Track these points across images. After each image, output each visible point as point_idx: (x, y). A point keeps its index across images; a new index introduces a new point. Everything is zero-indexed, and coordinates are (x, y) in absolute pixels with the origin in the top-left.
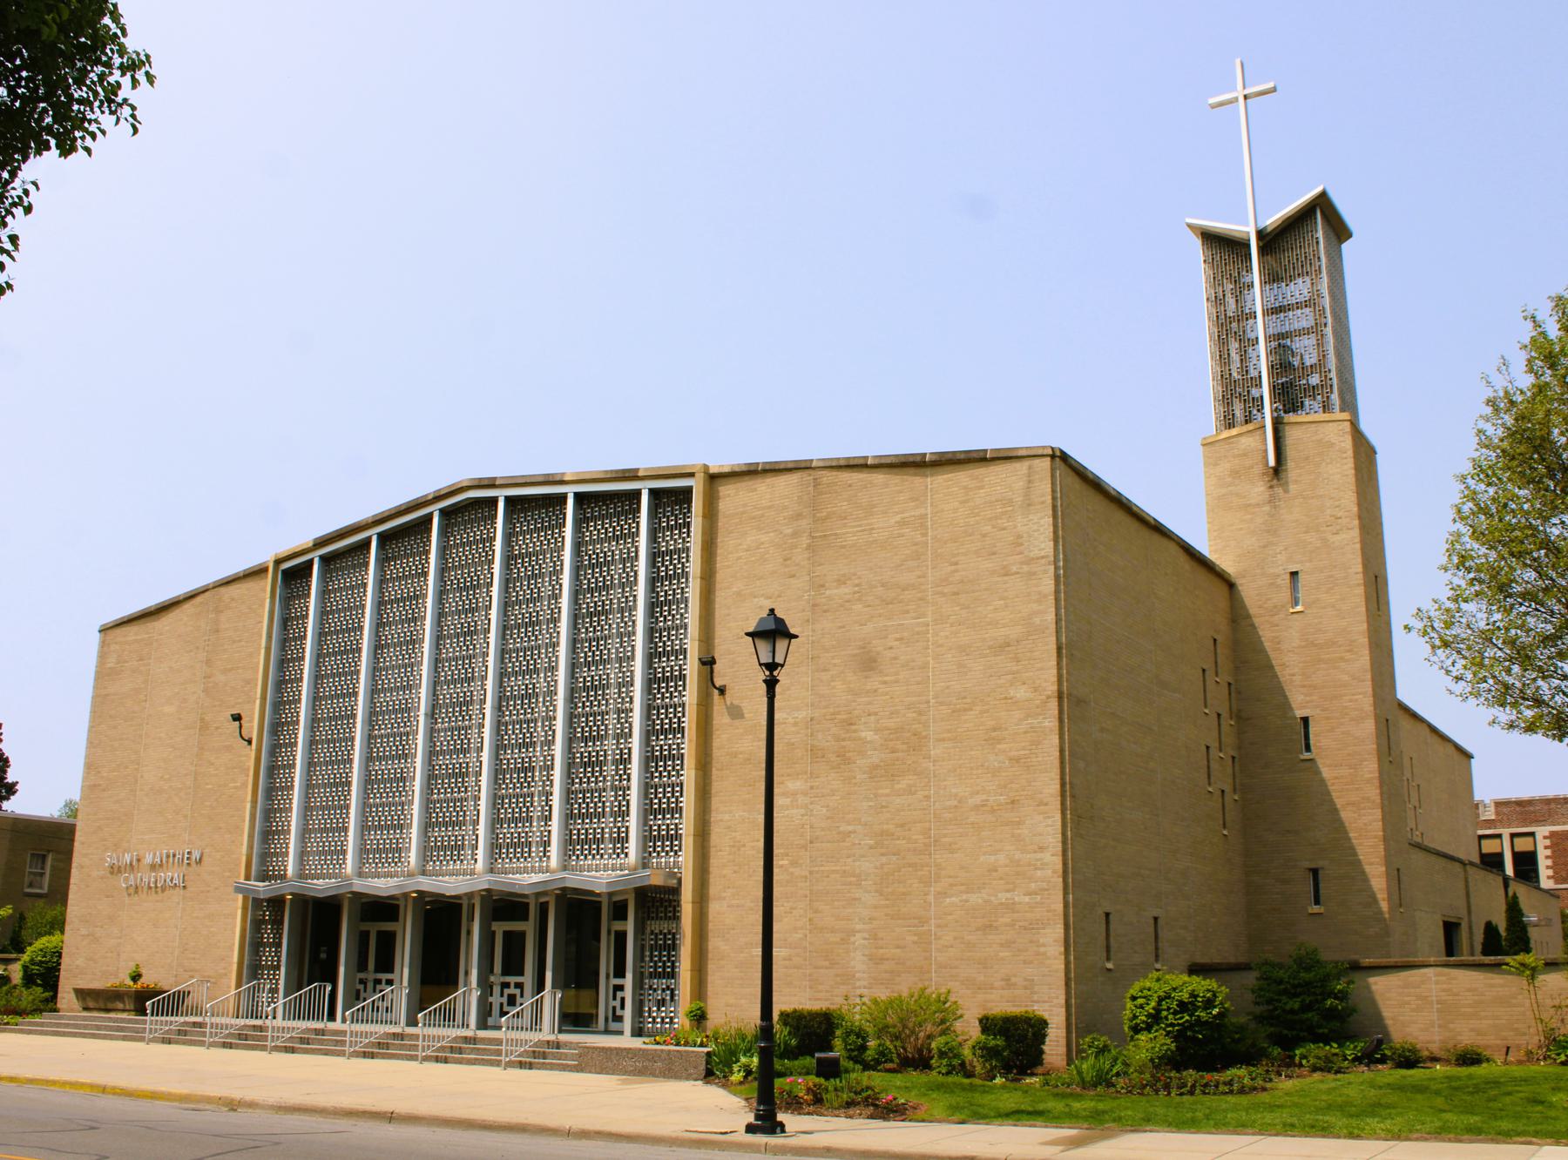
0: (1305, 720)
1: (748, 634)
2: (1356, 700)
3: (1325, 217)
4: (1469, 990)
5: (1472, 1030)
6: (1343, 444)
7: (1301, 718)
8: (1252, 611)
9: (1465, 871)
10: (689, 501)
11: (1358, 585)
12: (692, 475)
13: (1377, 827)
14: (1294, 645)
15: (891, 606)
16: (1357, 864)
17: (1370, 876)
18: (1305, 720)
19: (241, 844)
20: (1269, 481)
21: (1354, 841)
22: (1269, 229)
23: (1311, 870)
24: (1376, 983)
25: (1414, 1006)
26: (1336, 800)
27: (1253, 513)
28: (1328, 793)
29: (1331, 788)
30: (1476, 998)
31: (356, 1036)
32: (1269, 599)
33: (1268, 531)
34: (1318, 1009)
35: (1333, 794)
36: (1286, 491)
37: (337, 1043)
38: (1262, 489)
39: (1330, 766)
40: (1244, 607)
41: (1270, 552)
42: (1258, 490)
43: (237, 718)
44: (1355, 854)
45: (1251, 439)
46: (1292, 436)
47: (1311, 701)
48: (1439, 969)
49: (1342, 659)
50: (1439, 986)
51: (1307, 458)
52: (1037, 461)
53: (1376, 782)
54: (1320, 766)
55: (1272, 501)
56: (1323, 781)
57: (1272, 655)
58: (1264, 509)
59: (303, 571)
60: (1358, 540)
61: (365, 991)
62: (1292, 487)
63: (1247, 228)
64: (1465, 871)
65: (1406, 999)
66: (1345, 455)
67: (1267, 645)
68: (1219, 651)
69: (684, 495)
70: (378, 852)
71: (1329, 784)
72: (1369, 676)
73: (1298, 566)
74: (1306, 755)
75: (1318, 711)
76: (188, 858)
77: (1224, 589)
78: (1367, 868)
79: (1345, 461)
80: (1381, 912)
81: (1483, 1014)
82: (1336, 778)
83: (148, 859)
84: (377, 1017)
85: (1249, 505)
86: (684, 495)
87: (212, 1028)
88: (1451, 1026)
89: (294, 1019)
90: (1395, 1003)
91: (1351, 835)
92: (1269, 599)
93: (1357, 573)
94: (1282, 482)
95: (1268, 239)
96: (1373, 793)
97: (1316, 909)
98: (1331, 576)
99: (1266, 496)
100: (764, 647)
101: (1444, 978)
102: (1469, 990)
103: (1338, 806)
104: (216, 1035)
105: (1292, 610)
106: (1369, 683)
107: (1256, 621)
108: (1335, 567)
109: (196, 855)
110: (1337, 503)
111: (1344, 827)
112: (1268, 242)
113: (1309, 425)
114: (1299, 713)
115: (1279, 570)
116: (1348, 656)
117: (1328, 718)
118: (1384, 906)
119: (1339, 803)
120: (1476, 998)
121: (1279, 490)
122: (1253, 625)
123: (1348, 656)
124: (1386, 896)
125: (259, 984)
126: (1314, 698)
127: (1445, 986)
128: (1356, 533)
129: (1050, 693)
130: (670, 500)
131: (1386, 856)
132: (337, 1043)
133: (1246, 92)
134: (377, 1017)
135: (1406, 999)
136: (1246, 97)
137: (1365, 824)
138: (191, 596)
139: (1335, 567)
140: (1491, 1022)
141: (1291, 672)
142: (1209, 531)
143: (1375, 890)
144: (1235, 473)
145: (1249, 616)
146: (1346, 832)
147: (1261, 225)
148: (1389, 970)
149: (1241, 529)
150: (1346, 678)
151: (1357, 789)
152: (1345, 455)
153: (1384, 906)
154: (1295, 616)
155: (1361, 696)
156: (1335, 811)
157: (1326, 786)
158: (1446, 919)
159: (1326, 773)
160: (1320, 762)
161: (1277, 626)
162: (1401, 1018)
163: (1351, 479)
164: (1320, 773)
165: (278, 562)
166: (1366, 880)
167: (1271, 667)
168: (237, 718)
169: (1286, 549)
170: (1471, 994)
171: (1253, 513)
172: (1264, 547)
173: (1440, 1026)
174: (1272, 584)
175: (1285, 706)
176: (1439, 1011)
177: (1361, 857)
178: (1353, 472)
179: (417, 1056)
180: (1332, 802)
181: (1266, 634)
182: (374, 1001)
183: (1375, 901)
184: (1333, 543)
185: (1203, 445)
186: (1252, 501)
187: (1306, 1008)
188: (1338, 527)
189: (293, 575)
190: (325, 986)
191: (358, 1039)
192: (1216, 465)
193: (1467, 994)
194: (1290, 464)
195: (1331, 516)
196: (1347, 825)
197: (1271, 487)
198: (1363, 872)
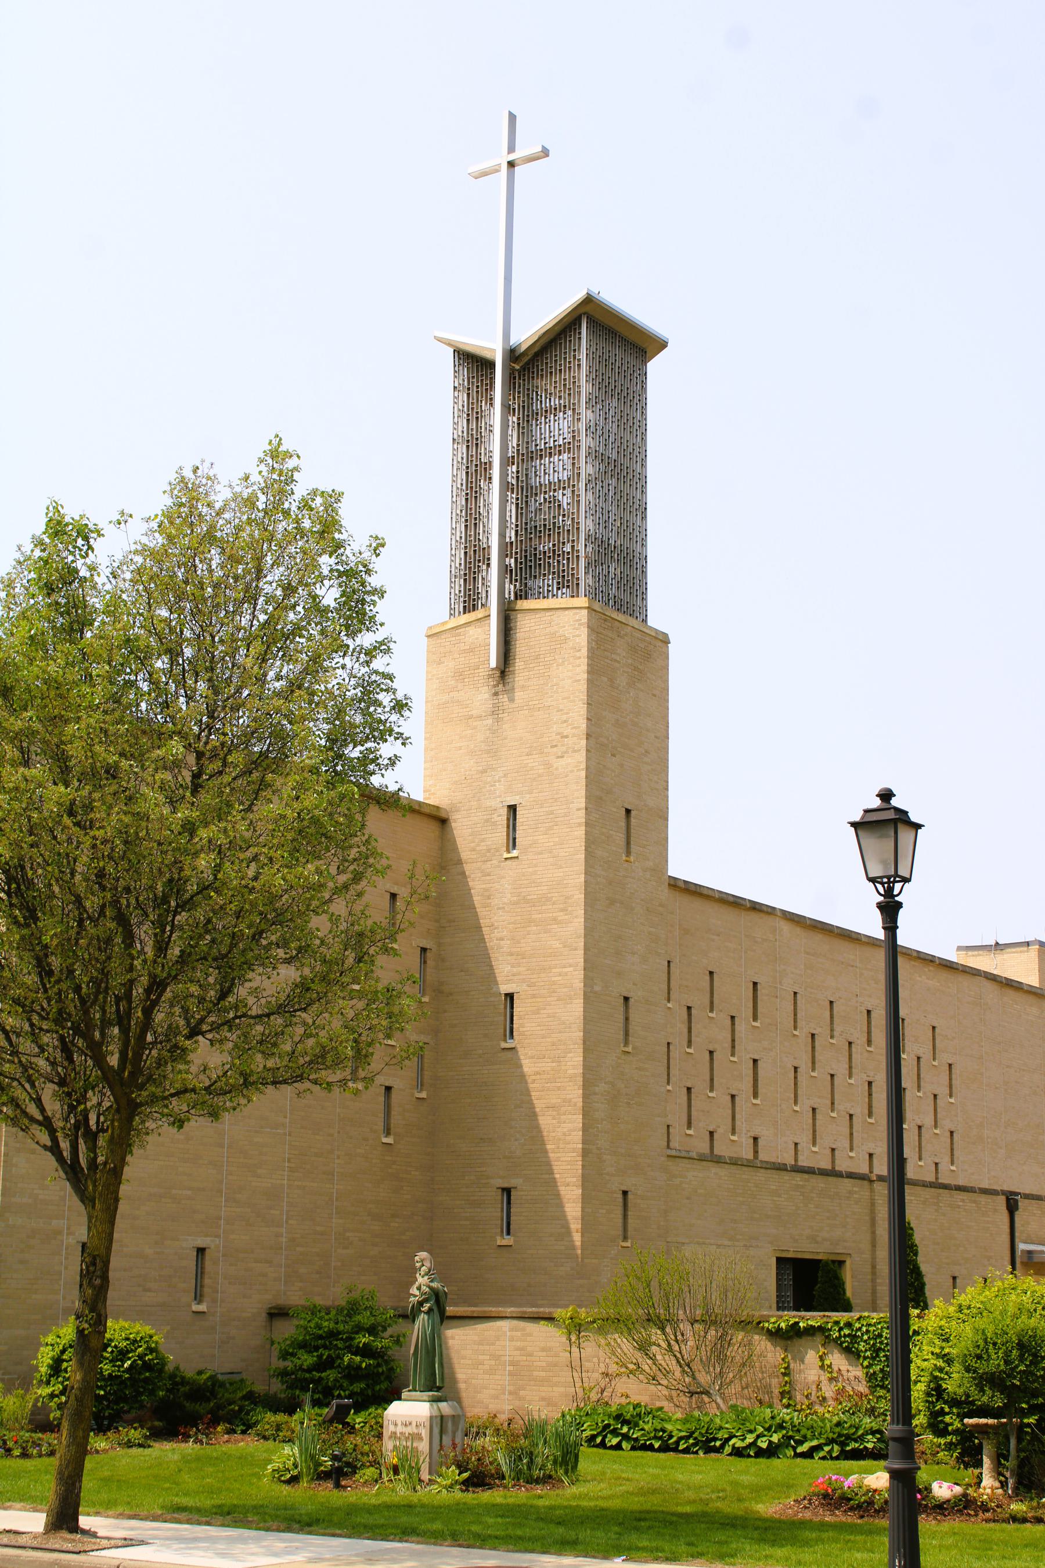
0: (510, 997)
1: (849, 823)
2: (566, 974)
3: (593, 322)
4: (543, 1350)
5: (543, 1399)
6: (577, 640)
7: (506, 995)
8: (465, 855)
9: (872, 1191)
11: (579, 825)
13: (576, 1137)
14: (505, 900)
16: (552, 1183)
17: (565, 1201)
18: (510, 997)
20: (495, 686)
21: (551, 1155)
22: (524, 348)
23: (503, 1189)
24: (453, 1338)
25: (488, 1367)
26: (535, 1102)
27: (475, 728)
28: (527, 1093)
29: (531, 1086)
30: (550, 1359)
32: (483, 840)
33: (488, 752)
34: (339, 1366)
35: (533, 1094)
36: (512, 700)
38: (487, 696)
39: (532, 1057)
40: (455, 849)
41: (489, 779)
42: (481, 696)
44: (551, 1172)
45: (479, 630)
46: (525, 626)
47: (519, 974)
48: (515, 1322)
49: (555, 919)
50: (514, 1343)
51: (537, 657)
53: (580, 1080)
54: (522, 1057)
55: (496, 712)
56: (522, 1077)
57: (481, 911)
58: (485, 722)
60: (583, 766)
62: (518, 695)
63: (494, 349)
64: (872, 1191)
65: (481, 1357)
66: (578, 654)
67: (477, 899)
71: (529, 1081)
72: (581, 944)
73: (517, 797)
74: (509, 1044)
75: (524, 987)
77: (431, 829)
78: (563, 1190)
79: (578, 662)
80: (574, 1248)
81: (555, 1379)
82: (537, 1073)
85: (471, 717)
88: (522, 1393)
90: (470, 1362)
91: (548, 1147)
92: (483, 840)
93: (578, 810)
94: (507, 688)
95: (526, 359)
96: (576, 1094)
97: (508, 1240)
98: (552, 813)
99: (489, 706)
100: (880, 845)
101: (519, 1334)
102: (543, 1350)
103: (537, 1110)
105: (506, 855)
106: (581, 952)
107: (468, 868)
108: (556, 800)
110: (564, 717)
111: (542, 1136)
112: (527, 363)
113: (542, 614)
114: (505, 989)
115: (495, 803)
116: (561, 916)
117: (534, 996)
118: (577, 1238)
119: (539, 1105)
120: (550, 1359)
121: (504, 698)
122: (463, 873)
123: (561, 916)
124: (580, 1226)
126: (521, 969)
127: (519, 1344)
128: (582, 756)
131: (583, 1175)
133: (511, 157)
135: (481, 1357)
136: (511, 164)
137: (564, 1134)
139: (556, 800)
140: (562, 1389)
141: (499, 935)
142: (426, 749)
143: (569, 1218)
144: (459, 675)
145: (459, 862)
146: (543, 1144)
147: (514, 341)
148: (467, 1321)
149: (460, 748)
150: (557, 944)
151: (559, 1088)
152: (578, 654)
153: (577, 1238)
154: (509, 862)
155: (571, 969)
156: (533, 1116)
157: (526, 1083)
158: (779, 1255)
159: (528, 1066)
160: (521, 1052)
161: (489, 875)
162: (474, 1381)
163: (583, 686)
164: (521, 1066)
166: (560, 1205)
167: (479, 928)
169: (505, 776)
170: (544, 1354)
171: (475, 728)
172: (484, 771)
173: (510, 1393)
174: (487, 821)
175: (490, 977)
176: (511, 1374)
177: (557, 1176)
178: (585, 676)
180: (532, 1107)
181: (477, 885)
183: (568, 1232)
184: (557, 769)
185: (428, 636)
186: (474, 713)
187: (322, 1365)
188: (564, 749)
192: (440, 663)
193: (540, 1354)
194: (519, 664)
195: (558, 734)
196: (545, 1134)
197: (496, 694)
198: (558, 1195)
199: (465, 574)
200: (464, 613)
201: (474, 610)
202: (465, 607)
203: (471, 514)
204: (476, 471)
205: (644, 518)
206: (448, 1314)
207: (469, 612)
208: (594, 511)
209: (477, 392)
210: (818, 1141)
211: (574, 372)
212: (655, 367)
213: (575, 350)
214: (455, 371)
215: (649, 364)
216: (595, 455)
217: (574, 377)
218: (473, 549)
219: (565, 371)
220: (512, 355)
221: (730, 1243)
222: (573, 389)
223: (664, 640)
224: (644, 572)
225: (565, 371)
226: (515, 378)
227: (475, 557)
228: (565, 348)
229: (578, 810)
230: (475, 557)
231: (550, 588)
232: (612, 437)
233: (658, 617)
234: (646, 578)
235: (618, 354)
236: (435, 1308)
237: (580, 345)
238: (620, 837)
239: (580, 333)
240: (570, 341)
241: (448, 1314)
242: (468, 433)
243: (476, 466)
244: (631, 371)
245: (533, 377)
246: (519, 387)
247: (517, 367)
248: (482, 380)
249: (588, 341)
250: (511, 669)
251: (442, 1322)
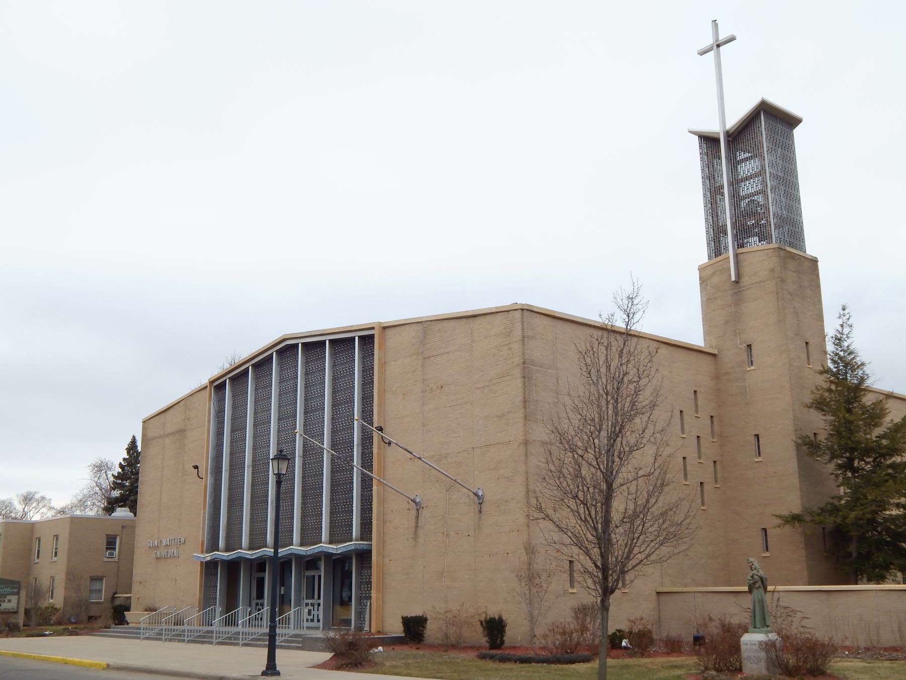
3: (766, 113)
10: (373, 342)
12: (373, 328)
15: (456, 395)
19: (201, 533)
31: (219, 633)
37: (136, 633)
43: (196, 467)
52: (515, 312)
59: (223, 384)
61: (314, 610)
68: (700, 403)
69: (372, 337)
70: (310, 535)
76: (180, 542)
83: (164, 543)
84: (255, 623)
86: (372, 337)
87: (188, 632)
89: (203, 626)
93: (518, 336)
104: (168, 636)
109: (183, 540)
125: (301, 609)
129: (521, 441)
130: (367, 341)
132: (136, 633)
134: (255, 623)
138: (183, 399)
165: (212, 382)
168: (196, 467)
179: (162, 638)
182: (256, 615)
189: (217, 386)
190: (247, 609)
191: (221, 635)
199: (714, 239)
200: (716, 257)
201: (720, 255)
202: (715, 254)
203: (714, 211)
204: (715, 190)
205: (799, 203)
206: (768, 590)
207: (718, 256)
208: (775, 202)
209: (712, 154)
210: (761, 454)
211: (760, 138)
212: (797, 131)
213: (759, 127)
214: (700, 146)
215: (794, 131)
216: (774, 177)
217: (760, 140)
218: (717, 227)
219: (750, 140)
220: (728, 134)
221: (657, 465)
222: (759, 146)
223: (814, 261)
224: (802, 229)
225: (750, 140)
226: (730, 144)
227: (718, 230)
228: (754, 127)
229: (518, 336)
230: (718, 230)
231: (755, 242)
232: (781, 167)
233: (812, 248)
234: (803, 231)
235: (780, 127)
236: (761, 586)
237: (761, 124)
238: (804, 356)
239: (760, 119)
240: (756, 123)
241: (768, 590)
242: (709, 173)
243: (715, 188)
244: (786, 134)
245: (739, 143)
246: (732, 148)
247: (731, 139)
248: (714, 148)
249: (765, 122)
250: (742, 281)
251: (765, 593)
